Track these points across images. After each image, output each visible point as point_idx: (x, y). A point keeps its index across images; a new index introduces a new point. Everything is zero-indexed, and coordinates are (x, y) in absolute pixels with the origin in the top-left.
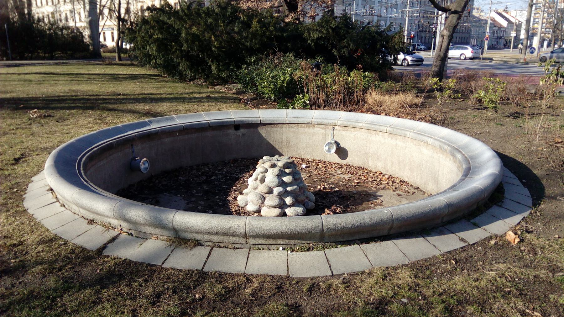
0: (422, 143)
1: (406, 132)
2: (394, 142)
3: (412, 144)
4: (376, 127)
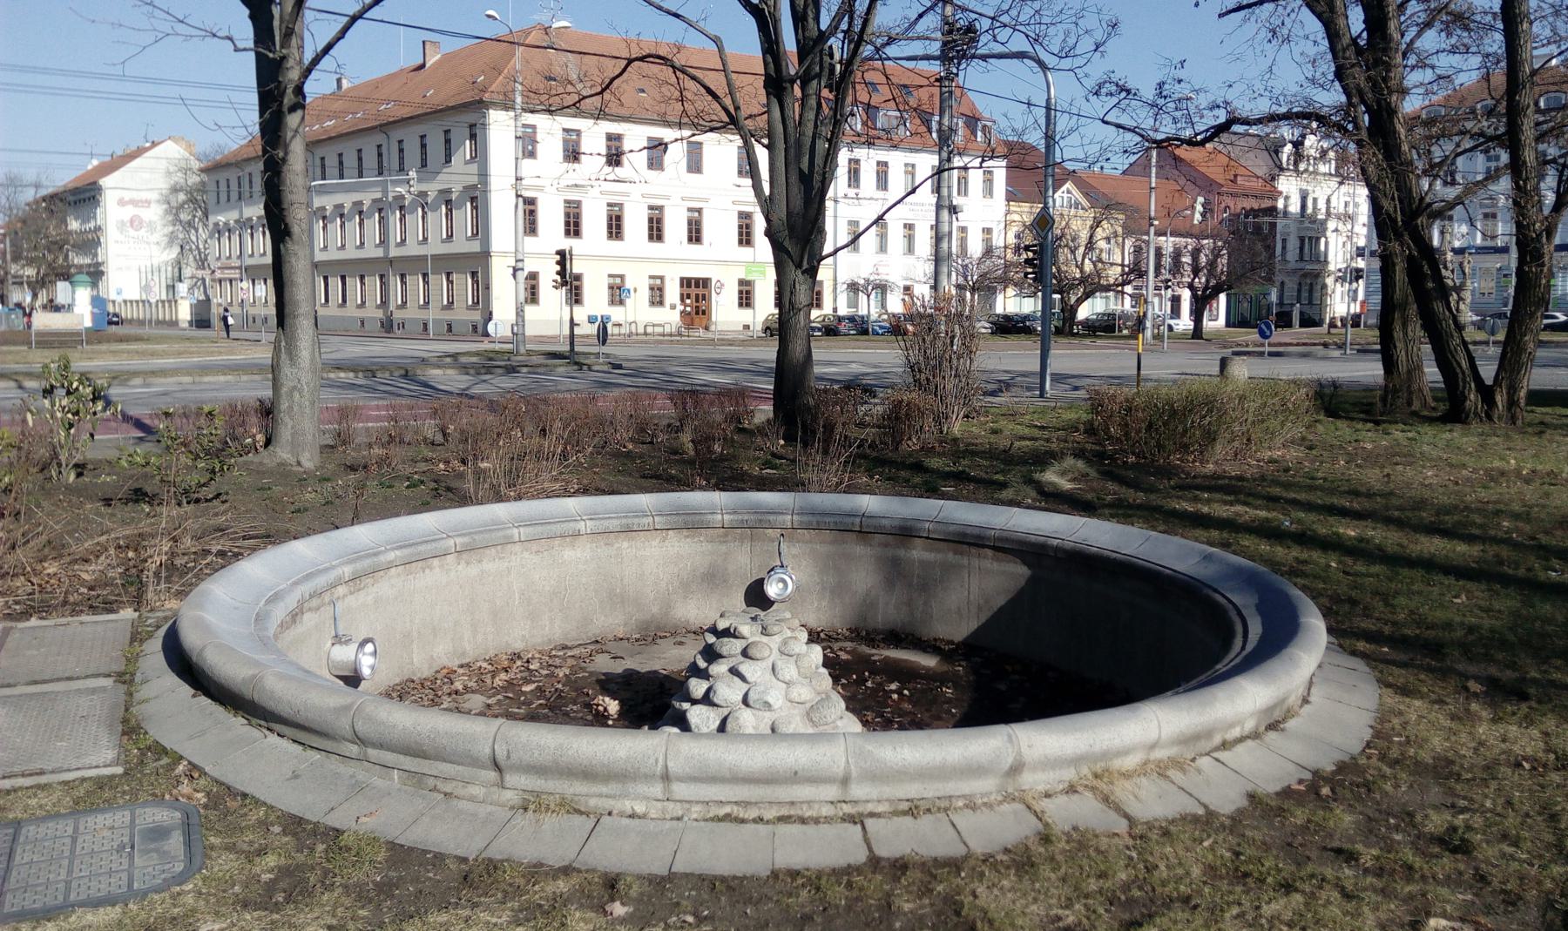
0: (557, 542)
1: (509, 532)
2: (473, 570)
3: (526, 555)
4: (429, 547)
